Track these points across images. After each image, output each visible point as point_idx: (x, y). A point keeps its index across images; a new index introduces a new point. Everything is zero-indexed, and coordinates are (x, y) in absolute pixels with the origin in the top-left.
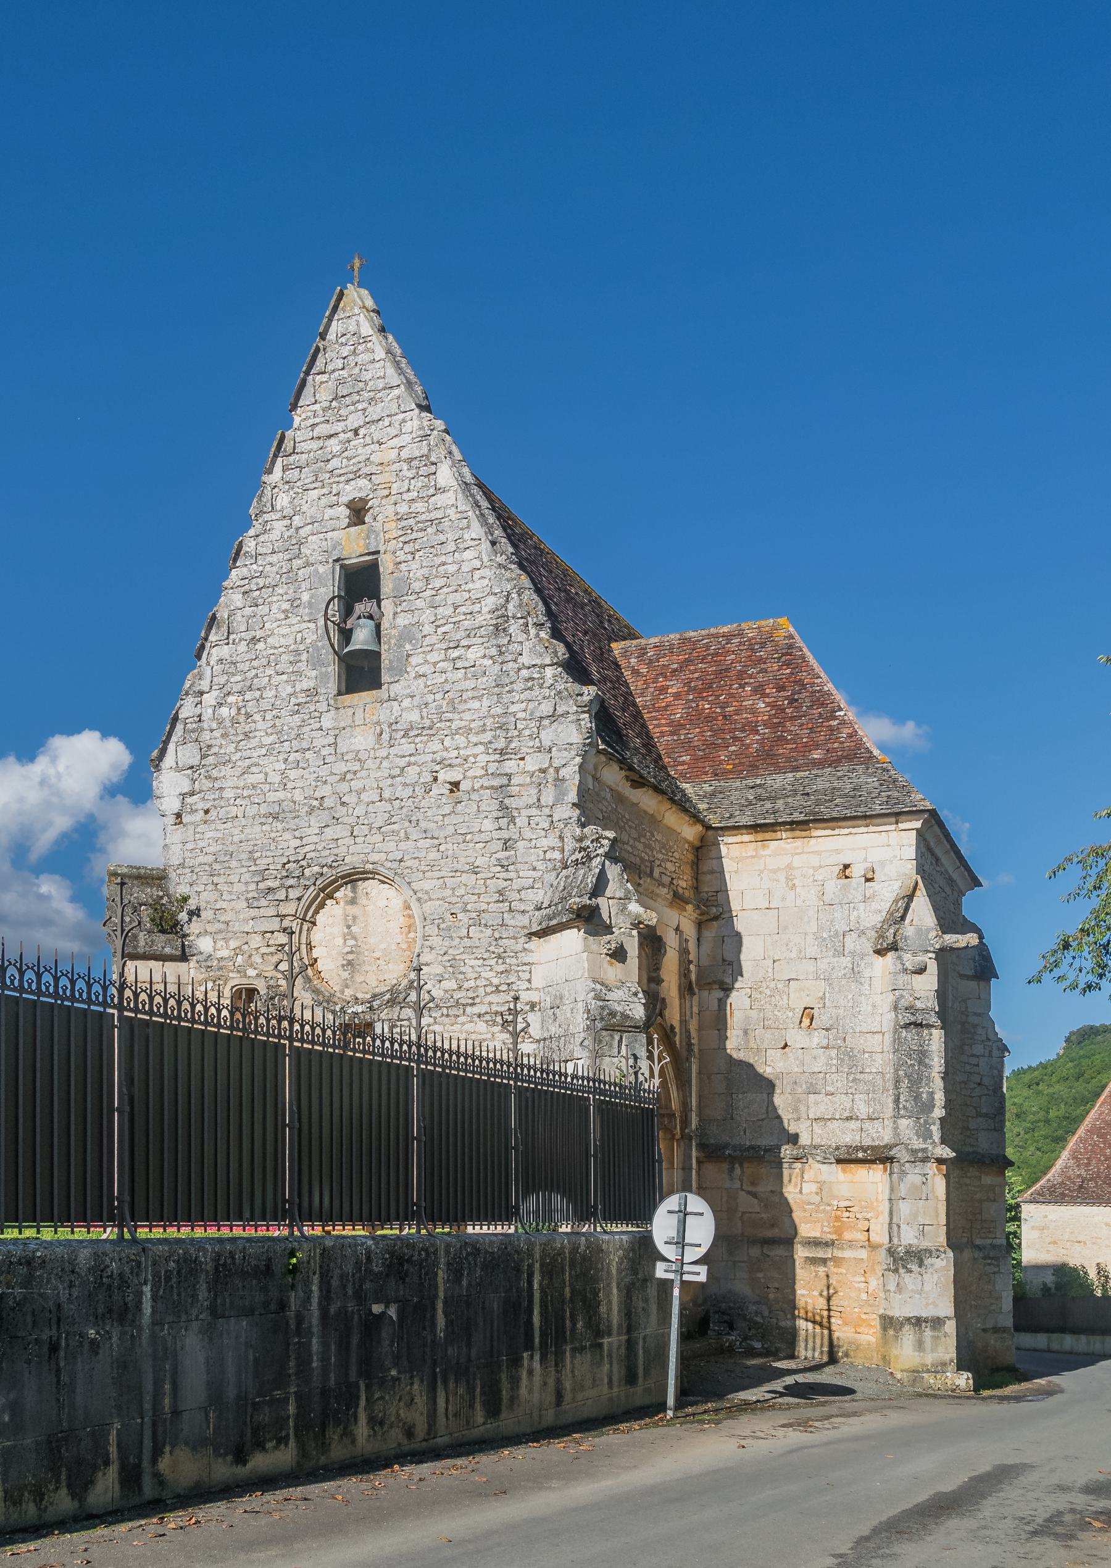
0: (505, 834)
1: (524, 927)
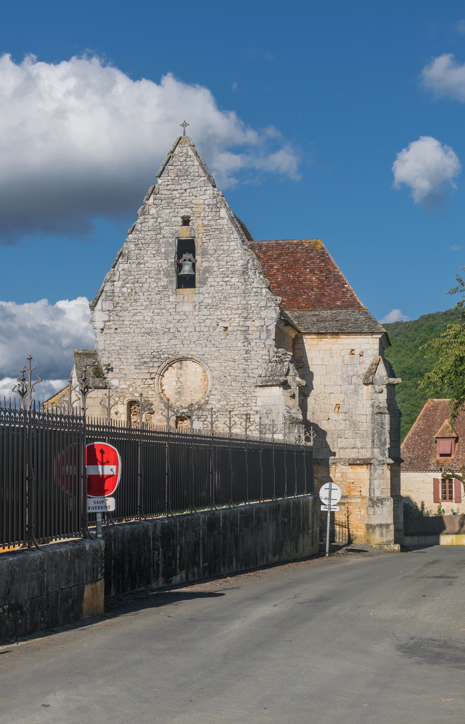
0: (246, 348)
1: (254, 383)
